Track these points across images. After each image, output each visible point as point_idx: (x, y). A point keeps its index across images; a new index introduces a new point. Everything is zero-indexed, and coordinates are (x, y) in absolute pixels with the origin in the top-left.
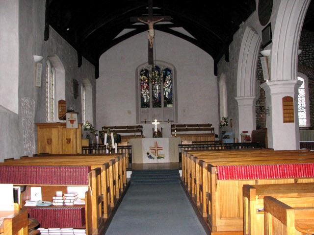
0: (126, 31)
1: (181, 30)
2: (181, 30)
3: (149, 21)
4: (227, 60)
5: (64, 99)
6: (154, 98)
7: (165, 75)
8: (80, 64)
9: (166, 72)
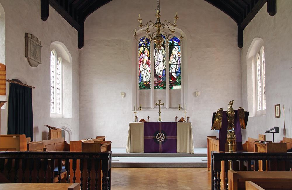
4: (272, 10)
6: (156, 76)
7: (172, 47)
8: (45, 15)
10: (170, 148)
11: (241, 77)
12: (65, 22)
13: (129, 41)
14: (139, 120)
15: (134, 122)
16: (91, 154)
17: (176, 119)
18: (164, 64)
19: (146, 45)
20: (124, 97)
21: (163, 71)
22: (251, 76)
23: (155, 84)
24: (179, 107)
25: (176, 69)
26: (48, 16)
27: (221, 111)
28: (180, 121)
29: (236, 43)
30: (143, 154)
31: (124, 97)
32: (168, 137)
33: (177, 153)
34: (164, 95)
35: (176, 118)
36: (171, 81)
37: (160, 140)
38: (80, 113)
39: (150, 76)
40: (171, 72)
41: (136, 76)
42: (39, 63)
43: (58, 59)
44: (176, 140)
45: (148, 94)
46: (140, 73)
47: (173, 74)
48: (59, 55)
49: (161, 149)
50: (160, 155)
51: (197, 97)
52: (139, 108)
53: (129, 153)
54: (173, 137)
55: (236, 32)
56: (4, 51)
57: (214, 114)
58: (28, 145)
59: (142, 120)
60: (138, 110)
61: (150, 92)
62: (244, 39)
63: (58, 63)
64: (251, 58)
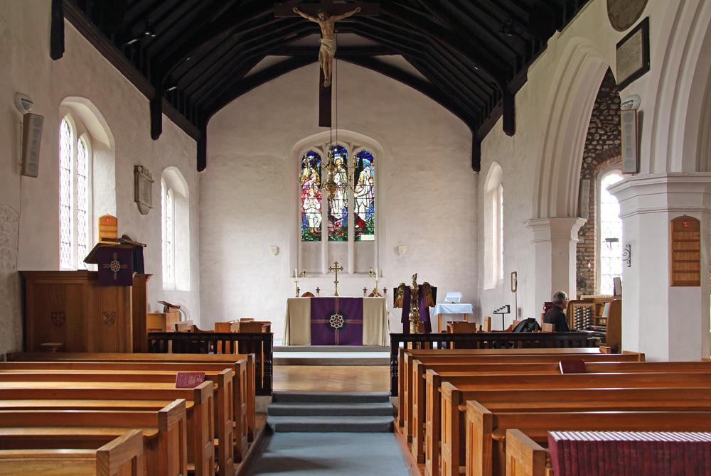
0: (269, 60)
1: (398, 60)
2: (398, 60)
3: (320, 15)
4: (510, 128)
5: (113, 213)
6: (332, 218)
7: (360, 168)
8: (156, 131)
9: (361, 161)
10: (352, 337)
11: (477, 221)
12: (180, 130)
13: (284, 158)
14: (301, 293)
15: (294, 297)
16: (251, 335)
17: (365, 292)
18: (345, 198)
19: (313, 164)
20: (276, 254)
21: (343, 210)
22: (491, 221)
23: (330, 232)
24: (371, 272)
25: (366, 206)
26: (160, 131)
27: (403, 286)
28: (372, 295)
29: (468, 162)
30: (309, 348)
31: (276, 254)
32: (349, 321)
33: (362, 345)
34: (344, 251)
35: (365, 290)
36: (357, 226)
37: (337, 326)
38: (200, 280)
39: (320, 218)
40: (356, 211)
41: (298, 220)
42: (150, 208)
43: (78, 137)
44: (362, 325)
45: (318, 250)
46: (304, 214)
47: (360, 215)
48: (81, 128)
49: (337, 338)
50: (336, 348)
51: (401, 255)
52: (301, 274)
53: (287, 345)
54: (357, 322)
55: (469, 145)
56: (115, 198)
57: (395, 289)
58: (176, 325)
59: (308, 294)
60: (300, 276)
61: (321, 245)
62: (482, 157)
63: (80, 148)
64: (491, 192)
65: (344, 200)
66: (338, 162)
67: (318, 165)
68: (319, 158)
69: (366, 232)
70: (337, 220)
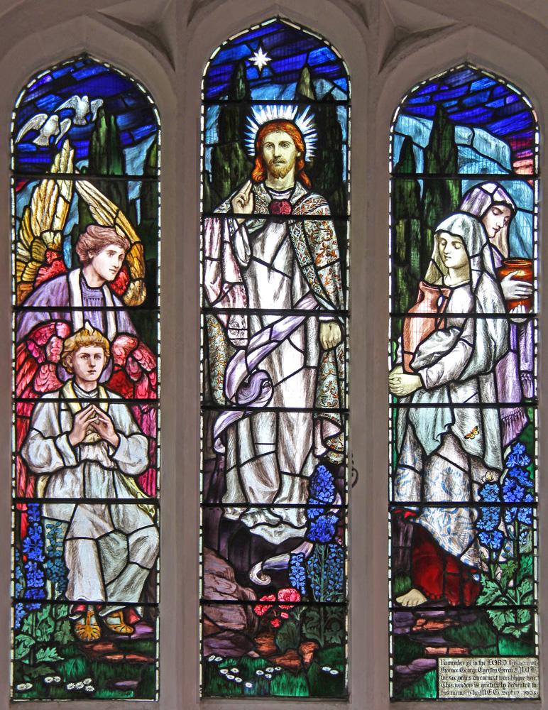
6: (230, 541)
7: (428, 191)
18: (330, 400)
21: (311, 485)
23: (213, 632)
36: (414, 598)
40: (407, 491)
46: (29, 506)
47: (436, 521)
55: (114, 16)
65: (316, 414)
66: (281, 149)
67: (135, 160)
68: (144, 114)
69: (481, 643)
70: (268, 550)
